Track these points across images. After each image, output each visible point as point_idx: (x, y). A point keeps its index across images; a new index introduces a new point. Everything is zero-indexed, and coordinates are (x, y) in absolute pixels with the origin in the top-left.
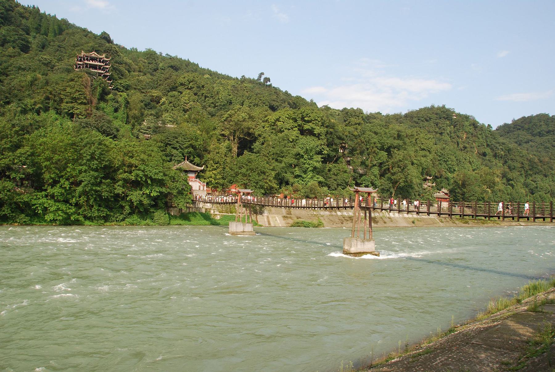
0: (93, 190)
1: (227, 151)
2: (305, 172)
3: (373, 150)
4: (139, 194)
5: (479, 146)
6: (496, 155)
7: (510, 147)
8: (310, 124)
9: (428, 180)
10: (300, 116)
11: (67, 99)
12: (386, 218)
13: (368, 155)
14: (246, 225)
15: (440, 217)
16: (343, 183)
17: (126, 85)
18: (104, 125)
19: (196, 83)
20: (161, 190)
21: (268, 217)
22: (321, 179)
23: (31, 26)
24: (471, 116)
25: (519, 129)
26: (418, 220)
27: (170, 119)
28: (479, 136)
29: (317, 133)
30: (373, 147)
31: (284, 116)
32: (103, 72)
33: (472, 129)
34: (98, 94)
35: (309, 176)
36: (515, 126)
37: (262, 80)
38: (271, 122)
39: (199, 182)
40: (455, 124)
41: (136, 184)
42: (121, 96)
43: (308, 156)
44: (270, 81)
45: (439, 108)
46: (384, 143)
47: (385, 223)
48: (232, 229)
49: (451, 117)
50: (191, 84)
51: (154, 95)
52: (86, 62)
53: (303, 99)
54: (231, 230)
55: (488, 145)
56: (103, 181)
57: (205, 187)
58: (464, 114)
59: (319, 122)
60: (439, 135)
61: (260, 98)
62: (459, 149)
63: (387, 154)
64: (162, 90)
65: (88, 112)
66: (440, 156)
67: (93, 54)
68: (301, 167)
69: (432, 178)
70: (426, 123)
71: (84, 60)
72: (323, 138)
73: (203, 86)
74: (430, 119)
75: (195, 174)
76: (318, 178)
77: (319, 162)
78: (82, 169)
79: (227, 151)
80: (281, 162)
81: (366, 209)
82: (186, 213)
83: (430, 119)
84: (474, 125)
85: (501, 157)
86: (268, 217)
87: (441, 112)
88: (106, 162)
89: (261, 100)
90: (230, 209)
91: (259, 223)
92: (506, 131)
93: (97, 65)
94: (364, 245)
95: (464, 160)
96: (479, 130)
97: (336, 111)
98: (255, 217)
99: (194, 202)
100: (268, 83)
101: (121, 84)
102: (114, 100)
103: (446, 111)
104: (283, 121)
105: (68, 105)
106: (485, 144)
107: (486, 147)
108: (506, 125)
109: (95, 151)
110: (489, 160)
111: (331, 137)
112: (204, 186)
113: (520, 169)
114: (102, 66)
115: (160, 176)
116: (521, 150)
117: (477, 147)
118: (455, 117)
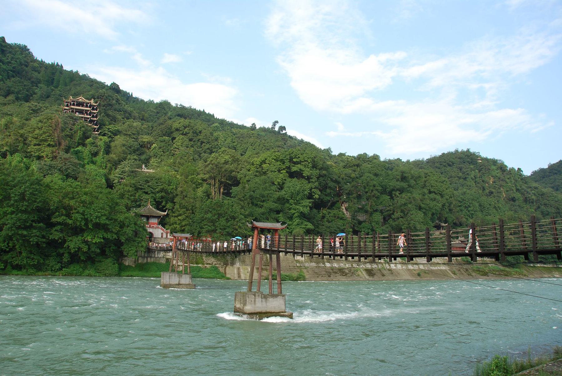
0: (19, 234)
1: (204, 196)
2: (291, 218)
3: (373, 194)
4: (78, 241)
5: (507, 191)
6: (526, 200)
7: (544, 191)
8: (299, 166)
9: (443, 227)
10: (288, 157)
11: (35, 142)
12: (385, 270)
13: (367, 199)
14: (183, 276)
15: (313, 258)
16: (337, 231)
17: (114, 130)
18: (68, 168)
19: (192, 129)
20: (106, 235)
21: (239, 269)
22: (310, 226)
23: (42, 79)
24: (500, 160)
25: (556, 174)
26: (425, 273)
27: (156, 164)
28: (508, 180)
29: (306, 175)
30: (372, 191)
31: (271, 158)
32: (89, 117)
33: (498, 173)
34: (78, 138)
35: (295, 223)
36: (551, 170)
37: (277, 129)
38: (256, 164)
39: (162, 229)
40: (481, 168)
41: (77, 231)
42: (101, 140)
43: (294, 200)
44: (285, 130)
45: (463, 152)
46: (385, 186)
47: (383, 275)
48: (164, 281)
49: (476, 162)
50: (186, 129)
51: (144, 140)
52: (73, 107)
53: (313, 145)
54: (163, 282)
55: (517, 190)
56: (34, 224)
57: (169, 234)
58: (492, 158)
59: (309, 163)
60: (462, 180)
61: (264, 144)
62: (485, 195)
63: (389, 198)
64: (155, 136)
65: (54, 154)
66: (460, 201)
67: (80, 99)
68: (285, 213)
69: (447, 224)
70: (448, 168)
71: (71, 105)
72: (314, 180)
73: (200, 132)
74: (453, 164)
75: (158, 219)
76: (306, 225)
77: (307, 207)
78: (7, 211)
79: (204, 196)
80: (261, 207)
81: (270, 252)
82: (144, 263)
83: (453, 164)
84: (501, 168)
85: (532, 203)
86: (239, 269)
87: (465, 156)
88: (38, 203)
89: (265, 146)
90: (197, 259)
91: (228, 276)
92: (541, 175)
93: (83, 110)
94: (266, 301)
95: (488, 206)
96: (507, 174)
97: (348, 157)
98: (224, 269)
99: (149, 251)
100: (284, 132)
101: (109, 129)
102: (94, 144)
103: (471, 155)
104: (269, 164)
105: (35, 147)
106: (514, 189)
107: (515, 191)
108: (542, 170)
109: (26, 191)
110: (519, 206)
111: (324, 180)
112: (167, 233)
113: (554, 215)
114: (88, 111)
115: (103, 220)
116: (555, 194)
117: (505, 192)
118: (480, 161)
